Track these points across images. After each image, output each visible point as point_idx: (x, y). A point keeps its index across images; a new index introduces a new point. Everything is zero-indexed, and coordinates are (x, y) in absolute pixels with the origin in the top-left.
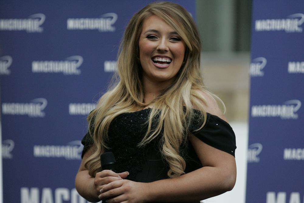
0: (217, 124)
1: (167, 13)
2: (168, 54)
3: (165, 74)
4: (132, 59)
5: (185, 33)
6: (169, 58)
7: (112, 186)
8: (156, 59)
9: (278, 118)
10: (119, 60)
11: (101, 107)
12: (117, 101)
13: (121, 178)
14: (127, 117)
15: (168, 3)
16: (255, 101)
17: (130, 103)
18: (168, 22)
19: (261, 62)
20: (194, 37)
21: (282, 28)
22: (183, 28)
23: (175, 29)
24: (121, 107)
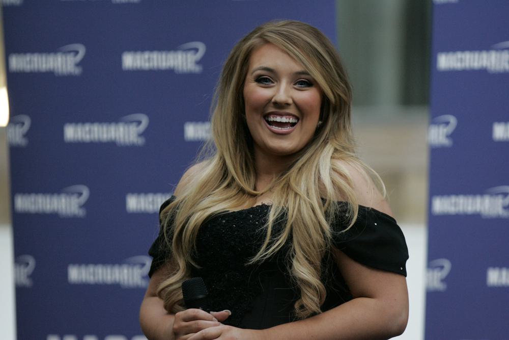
0: (376, 224)
1: (289, 41)
2: (292, 110)
3: (287, 144)
4: (233, 119)
5: (321, 73)
6: (294, 116)
7: (203, 336)
8: (271, 117)
9: (476, 218)
10: (213, 119)
11: (186, 197)
12: (214, 187)
13: (217, 322)
14: (227, 219)
15: (293, 22)
16: (437, 188)
17: (235, 190)
18: (292, 54)
19: (447, 123)
20: (338, 79)
21: (482, 67)
22: (318, 65)
23: (304, 67)
24: (220, 198)
